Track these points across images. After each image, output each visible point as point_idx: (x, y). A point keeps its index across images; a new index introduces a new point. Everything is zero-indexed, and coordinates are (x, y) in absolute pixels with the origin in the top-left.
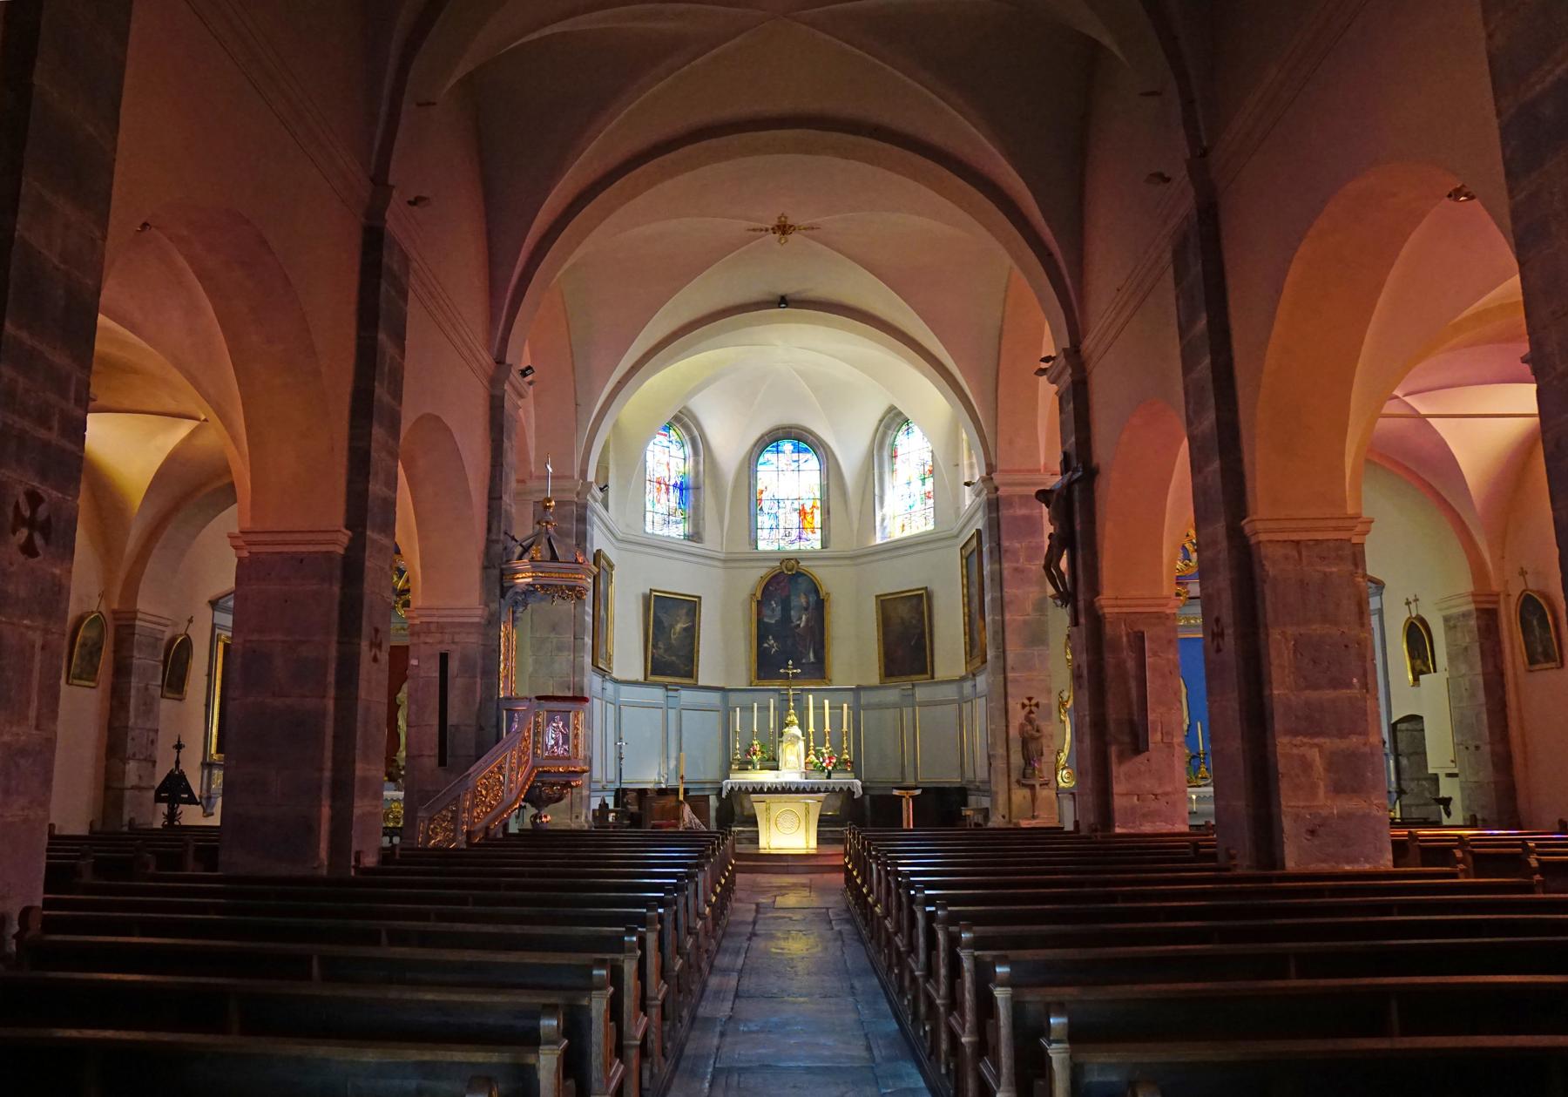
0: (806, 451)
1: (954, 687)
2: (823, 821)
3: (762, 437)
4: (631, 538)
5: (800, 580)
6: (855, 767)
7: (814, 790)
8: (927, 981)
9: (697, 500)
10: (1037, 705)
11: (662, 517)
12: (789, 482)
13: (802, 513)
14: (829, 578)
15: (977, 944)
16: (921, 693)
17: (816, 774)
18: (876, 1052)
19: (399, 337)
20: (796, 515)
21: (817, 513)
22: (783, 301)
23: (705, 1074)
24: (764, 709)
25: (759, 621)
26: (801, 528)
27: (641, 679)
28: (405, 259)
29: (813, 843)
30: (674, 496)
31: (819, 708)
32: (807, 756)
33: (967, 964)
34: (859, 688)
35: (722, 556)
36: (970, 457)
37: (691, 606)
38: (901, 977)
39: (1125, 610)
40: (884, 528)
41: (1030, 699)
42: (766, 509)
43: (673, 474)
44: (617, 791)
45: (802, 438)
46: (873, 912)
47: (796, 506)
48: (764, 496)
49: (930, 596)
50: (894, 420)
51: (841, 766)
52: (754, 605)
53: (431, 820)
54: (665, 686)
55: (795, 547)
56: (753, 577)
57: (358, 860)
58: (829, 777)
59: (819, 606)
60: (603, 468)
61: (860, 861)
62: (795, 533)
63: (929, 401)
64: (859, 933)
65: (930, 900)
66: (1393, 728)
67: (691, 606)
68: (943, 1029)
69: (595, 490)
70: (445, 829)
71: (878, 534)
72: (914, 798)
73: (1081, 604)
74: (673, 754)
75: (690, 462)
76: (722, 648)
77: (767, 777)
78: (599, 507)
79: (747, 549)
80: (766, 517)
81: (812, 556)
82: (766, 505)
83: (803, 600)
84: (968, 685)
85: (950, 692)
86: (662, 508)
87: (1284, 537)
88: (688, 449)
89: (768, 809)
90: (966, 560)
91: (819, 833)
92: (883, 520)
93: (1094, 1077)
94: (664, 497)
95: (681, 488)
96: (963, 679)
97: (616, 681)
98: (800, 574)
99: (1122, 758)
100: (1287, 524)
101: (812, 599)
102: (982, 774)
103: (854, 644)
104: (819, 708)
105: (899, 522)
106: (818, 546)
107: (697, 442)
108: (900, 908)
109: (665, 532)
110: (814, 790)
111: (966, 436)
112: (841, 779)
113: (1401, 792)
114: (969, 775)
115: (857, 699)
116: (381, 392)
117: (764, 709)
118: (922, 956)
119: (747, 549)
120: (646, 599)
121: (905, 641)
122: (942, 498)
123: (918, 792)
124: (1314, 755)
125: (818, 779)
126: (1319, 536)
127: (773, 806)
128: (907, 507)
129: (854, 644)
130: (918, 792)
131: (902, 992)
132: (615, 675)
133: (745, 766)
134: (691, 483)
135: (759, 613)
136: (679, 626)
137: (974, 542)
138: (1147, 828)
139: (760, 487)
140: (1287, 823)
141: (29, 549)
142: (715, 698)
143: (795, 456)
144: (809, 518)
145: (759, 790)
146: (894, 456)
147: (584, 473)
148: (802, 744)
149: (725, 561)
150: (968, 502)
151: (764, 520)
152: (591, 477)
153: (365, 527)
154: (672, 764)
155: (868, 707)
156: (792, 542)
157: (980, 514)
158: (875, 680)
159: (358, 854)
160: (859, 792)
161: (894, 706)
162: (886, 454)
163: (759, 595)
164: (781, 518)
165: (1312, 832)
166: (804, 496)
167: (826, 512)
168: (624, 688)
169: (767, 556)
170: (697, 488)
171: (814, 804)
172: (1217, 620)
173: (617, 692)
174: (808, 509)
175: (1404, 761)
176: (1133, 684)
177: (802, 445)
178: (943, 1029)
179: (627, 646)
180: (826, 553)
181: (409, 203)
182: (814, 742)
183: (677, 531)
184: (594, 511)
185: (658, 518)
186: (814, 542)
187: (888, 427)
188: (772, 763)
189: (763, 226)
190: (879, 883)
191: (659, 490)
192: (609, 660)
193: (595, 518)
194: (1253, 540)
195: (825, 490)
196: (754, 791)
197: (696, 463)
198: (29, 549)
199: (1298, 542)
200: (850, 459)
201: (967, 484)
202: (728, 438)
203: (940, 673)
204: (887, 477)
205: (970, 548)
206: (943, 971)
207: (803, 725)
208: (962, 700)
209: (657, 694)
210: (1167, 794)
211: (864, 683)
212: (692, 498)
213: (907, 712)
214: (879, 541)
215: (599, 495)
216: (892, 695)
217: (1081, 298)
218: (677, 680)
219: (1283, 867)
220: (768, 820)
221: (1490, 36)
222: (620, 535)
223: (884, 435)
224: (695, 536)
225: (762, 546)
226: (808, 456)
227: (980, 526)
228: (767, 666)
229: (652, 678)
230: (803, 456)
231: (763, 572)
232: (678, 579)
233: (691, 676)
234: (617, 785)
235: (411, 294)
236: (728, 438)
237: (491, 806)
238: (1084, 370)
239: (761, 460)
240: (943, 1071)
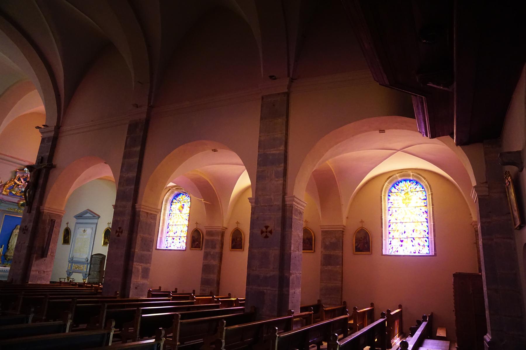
66: (92, 256)
87: (145, 211)
99: (37, 259)
100: (147, 208)
113: (89, 274)
124: (140, 268)
126: (152, 212)
138: (39, 282)
140: (132, 286)
141: (267, 227)
165: (136, 288)
175: (92, 266)
176: (47, 236)
194: (137, 210)
198: (267, 227)
199: (147, 213)
210: (47, 271)
217: (64, 114)
219: (128, 297)
221: (260, 136)
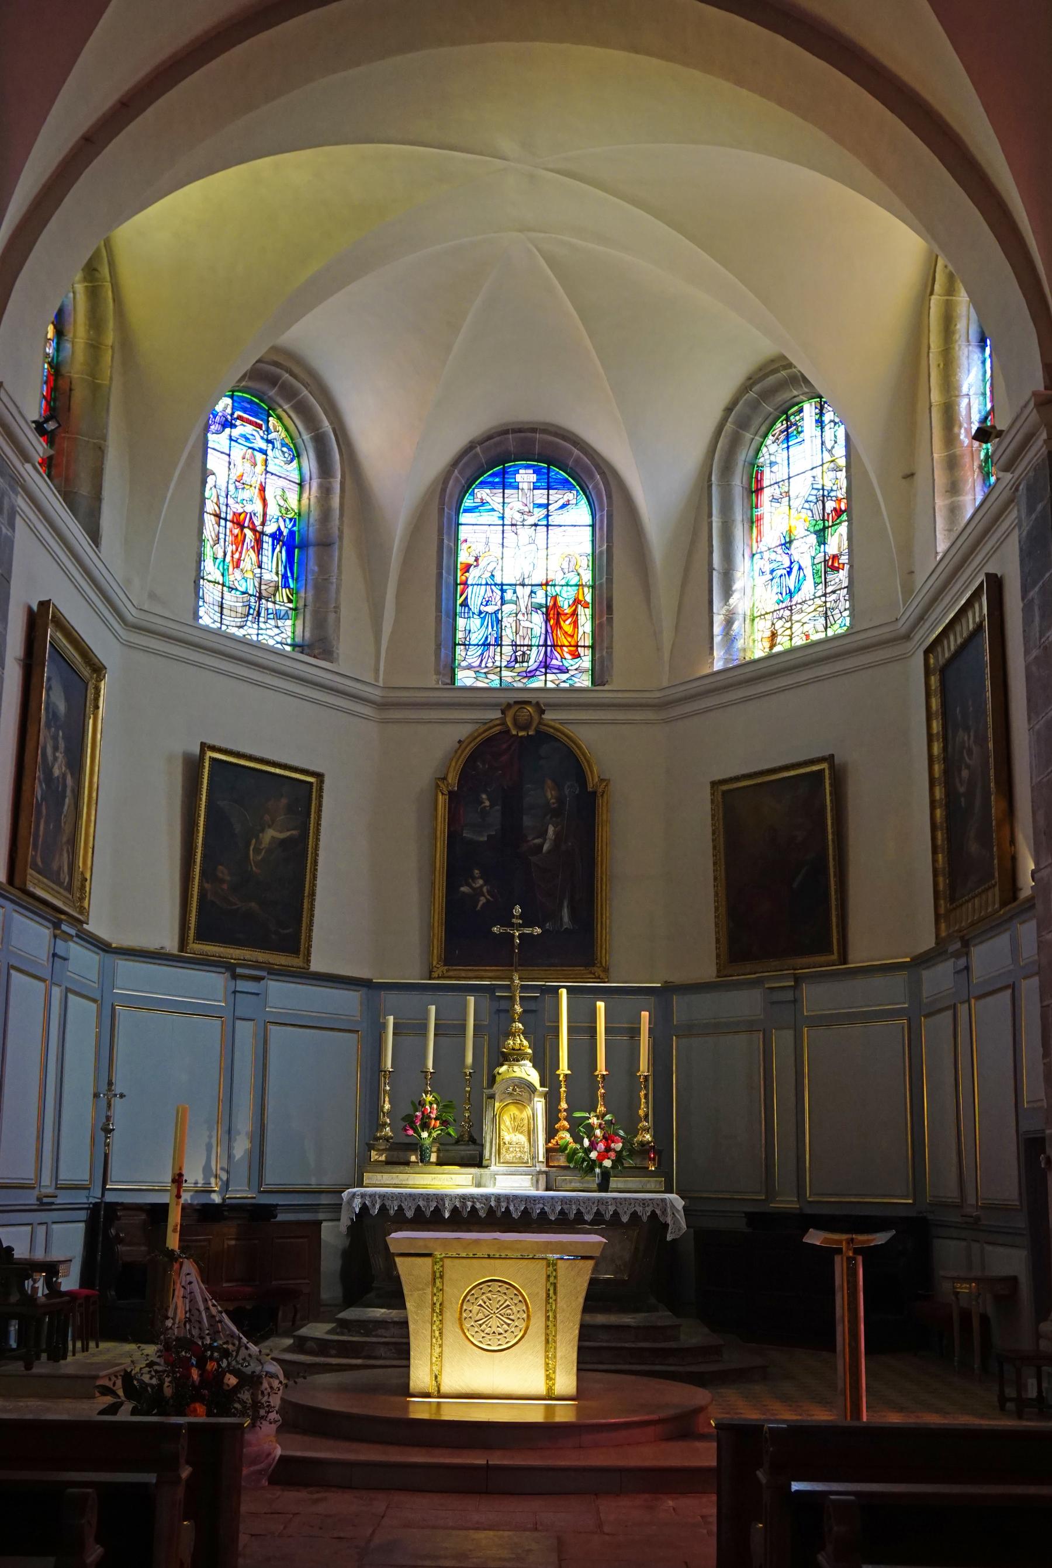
0: (565, 485)
1: (900, 978)
2: (596, 1298)
3: (471, 447)
7: (566, 1220)
9: (324, 567)
11: (236, 594)
12: (527, 549)
13: (552, 613)
14: (609, 750)
16: (816, 998)
17: (573, 1180)
20: (538, 619)
21: (585, 616)
24: (450, 1031)
25: (453, 838)
26: (550, 646)
27: (171, 945)
30: (273, 560)
31: (584, 1029)
32: (551, 1132)
34: (669, 990)
37: (298, 797)
40: (729, 639)
42: (474, 603)
43: (273, 510)
44: (95, 1209)
45: (557, 456)
47: (540, 598)
48: (473, 576)
49: (839, 776)
51: (633, 1159)
54: (231, 969)
55: (537, 683)
56: (440, 742)
58: (604, 1187)
59: (583, 805)
62: (535, 656)
67: (298, 797)
71: (718, 653)
72: (869, 1253)
74: (244, 1123)
76: (367, 889)
77: (454, 1182)
79: (432, 681)
80: (475, 622)
82: (475, 597)
83: (550, 795)
85: (891, 993)
86: (244, 580)
88: (309, 463)
89: (437, 1277)
91: (585, 1332)
92: (729, 622)
94: (249, 558)
96: (923, 961)
97: (103, 947)
103: (659, 886)
104: (584, 1029)
105: (763, 628)
106: (584, 681)
107: (328, 447)
109: (250, 631)
110: (566, 1220)
112: (632, 1192)
117: (450, 1031)
119: (432, 680)
120: (192, 767)
121: (780, 869)
123: (880, 1238)
125: (574, 1191)
127: (453, 1270)
128: (779, 590)
129: (659, 886)
130: (880, 1238)
133: (403, 1154)
134: (312, 535)
136: (270, 834)
139: (464, 557)
142: (350, 1001)
143: (540, 496)
144: (567, 626)
145: (433, 1214)
148: (539, 1104)
149: (383, 706)
150: (942, 547)
151: (471, 628)
154: (241, 1147)
155: (689, 1030)
156: (530, 675)
158: (706, 970)
160: (678, 1225)
161: (750, 1027)
162: (738, 482)
163: (453, 779)
164: (508, 622)
166: (558, 578)
167: (604, 607)
168: (124, 966)
169: (475, 699)
170: (325, 544)
171: (570, 1266)
173: (107, 978)
174: (565, 606)
179: (134, 861)
180: (604, 694)
182: (570, 1099)
183: (277, 634)
186: (578, 672)
187: (743, 424)
188: (469, 1152)
191: (239, 541)
192: (76, 886)
195: (603, 561)
196: (401, 1221)
197: (325, 491)
200: (657, 494)
202: (394, 439)
203: (860, 954)
204: (739, 532)
205: (970, 623)
207: (545, 1062)
208: (917, 1013)
209: (209, 986)
211: (678, 977)
212: (313, 566)
213: (782, 1040)
214: (718, 665)
216: (746, 1003)
218: (261, 956)
220: (439, 1310)
222: (132, 614)
223: (735, 443)
224: (317, 644)
225: (465, 678)
226: (570, 496)
228: (467, 937)
229: (198, 947)
230: (557, 497)
231: (464, 731)
232: (273, 733)
233: (295, 951)
236: (394, 439)
239: (468, 502)
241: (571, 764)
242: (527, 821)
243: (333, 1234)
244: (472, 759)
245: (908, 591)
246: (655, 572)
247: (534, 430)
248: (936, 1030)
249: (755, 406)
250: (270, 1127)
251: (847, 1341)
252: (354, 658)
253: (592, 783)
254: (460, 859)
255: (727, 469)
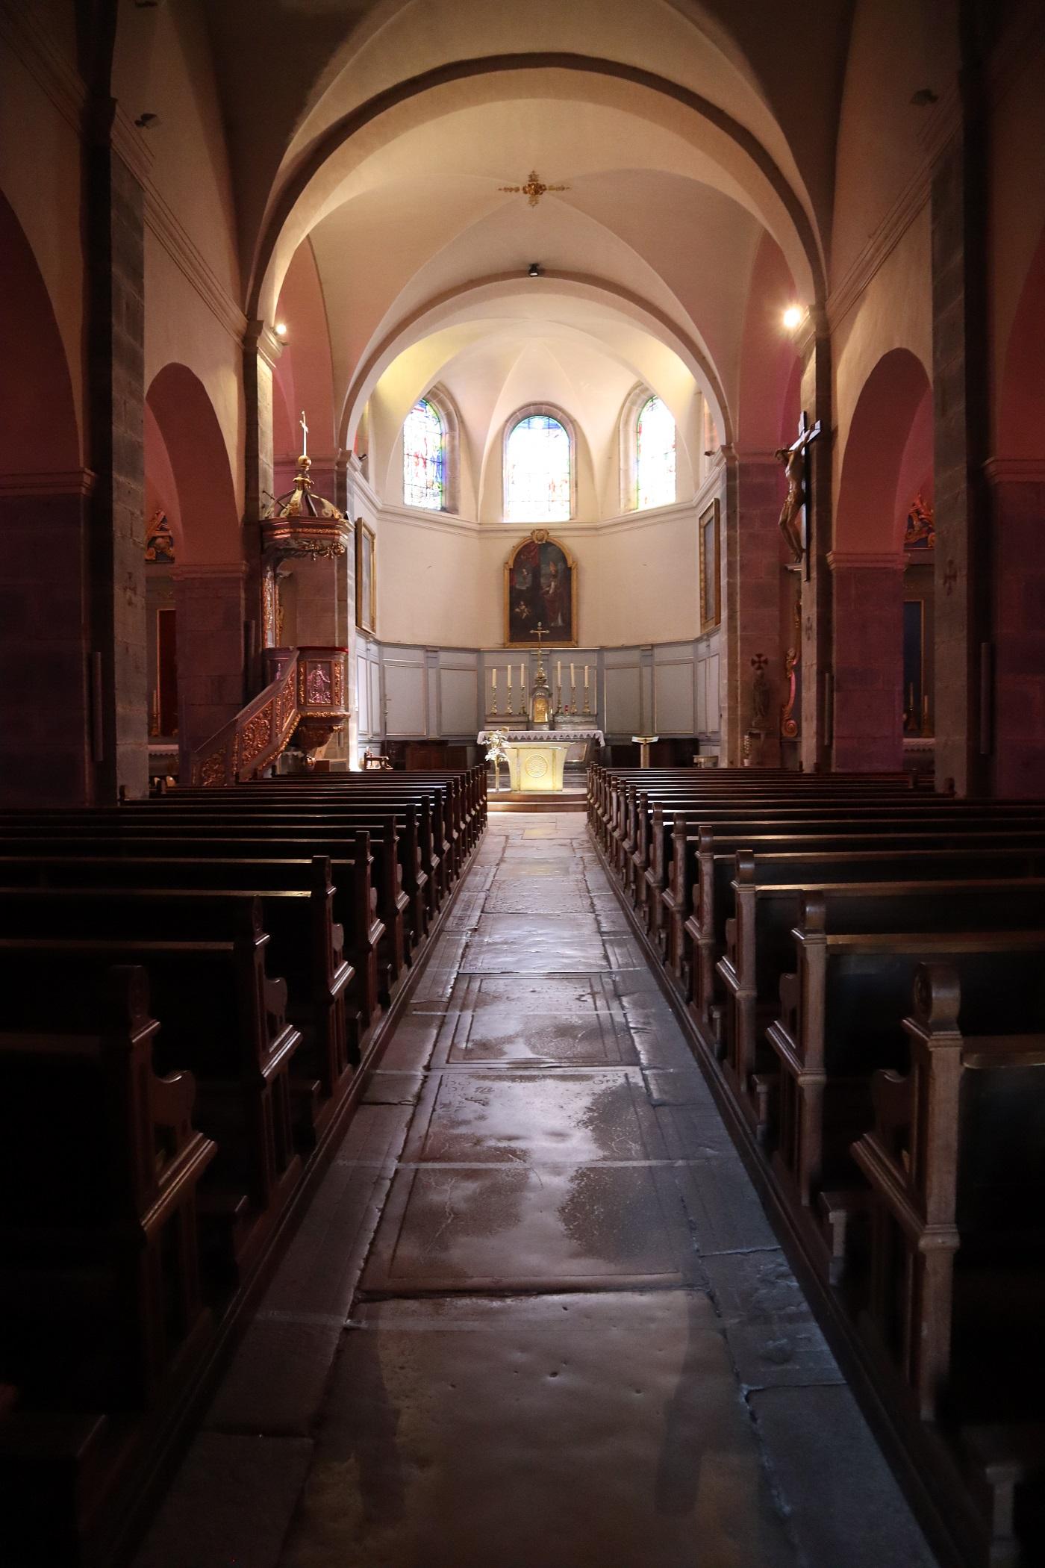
0: (556, 427)
1: (689, 649)
2: (568, 768)
4: (391, 509)
5: (550, 549)
6: (597, 720)
8: (663, 890)
10: (766, 662)
13: (553, 487)
15: (716, 848)
18: (612, 959)
19: (137, 275)
22: (535, 269)
23: (448, 982)
25: (512, 589)
28: (139, 187)
29: (559, 785)
30: (432, 469)
33: (707, 868)
35: (478, 527)
36: (711, 430)
38: (637, 892)
39: (857, 565)
41: (759, 656)
46: (612, 837)
50: (642, 395)
52: (507, 573)
53: (203, 764)
56: (505, 548)
57: (122, 794)
59: (566, 573)
60: (361, 438)
61: (600, 795)
63: (674, 374)
64: (600, 859)
65: (668, 817)
68: (679, 934)
69: (354, 458)
70: (216, 771)
73: (813, 559)
75: (447, 438)
78: (358, 476)
81: (563, 527)
84: (702, 646)
88: (445, 426)
90: (704, 528)
93: (853, 968)
95: (441, 463)
96: (698, 640)
97: (378, 643)
98: (549, 544)
101: (561, 566)
102: (716, 728)
108: (637, 827)
111: (709, 407)
114: (702, 728)
115: (601, 660)
116: (119, 329)
118: (660, 870)
122: (686, 470)
131: (637, 905)
132: (378, 636)
135: (511, 580)
137: (713, 511)
138: (865, 768)
146: (639, 432)
147: (343, 441)
149: (480, 532)
152: (350, 445)
153: (111, 470)
157: (719, 483)
159: (123, 788)
163: (511, 563)
172: (951, 562)
177: (553, 421)
178: (679, 934)
181: (138, 123)
184: (354, 480)
185: (416, 491)
187: (633, 403)
189: (514, 185)
190: (618, 809)
191: (417, 464)
193: (356, 488)
195: (575, 465)
197: (452, 438)
200: (597, 432)
201: (708, 454)
206: (680, 880)
215: (358, 464)
217: (828, 250)
222: (380, 506)
224: (451, 508)
227: (718, 496)
234: (382, 738)
235: (146, 229)
237: (258, 749)
238: (828, 328)
240: (678, 974)
241: (562, 556)
242: (543, 580)
243: (470, 750)
244: (519, 555)
245: (697, 485)
246: (594, 472)
247: (542, 404)
248: (701, 666)
249: (638, 395)
250: (444, 703)
251: (351, 573)
252: (467, 512)
253: (570, 562)
254: (515, 597)
255: (627, 423)
